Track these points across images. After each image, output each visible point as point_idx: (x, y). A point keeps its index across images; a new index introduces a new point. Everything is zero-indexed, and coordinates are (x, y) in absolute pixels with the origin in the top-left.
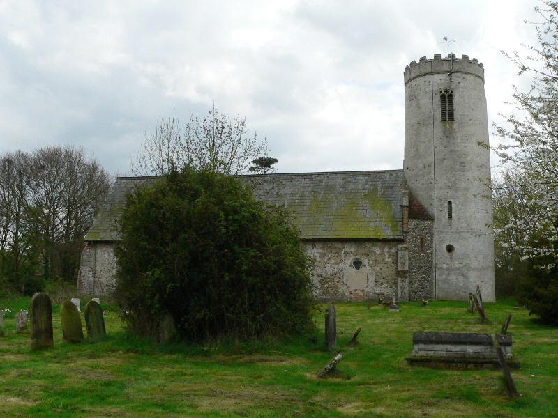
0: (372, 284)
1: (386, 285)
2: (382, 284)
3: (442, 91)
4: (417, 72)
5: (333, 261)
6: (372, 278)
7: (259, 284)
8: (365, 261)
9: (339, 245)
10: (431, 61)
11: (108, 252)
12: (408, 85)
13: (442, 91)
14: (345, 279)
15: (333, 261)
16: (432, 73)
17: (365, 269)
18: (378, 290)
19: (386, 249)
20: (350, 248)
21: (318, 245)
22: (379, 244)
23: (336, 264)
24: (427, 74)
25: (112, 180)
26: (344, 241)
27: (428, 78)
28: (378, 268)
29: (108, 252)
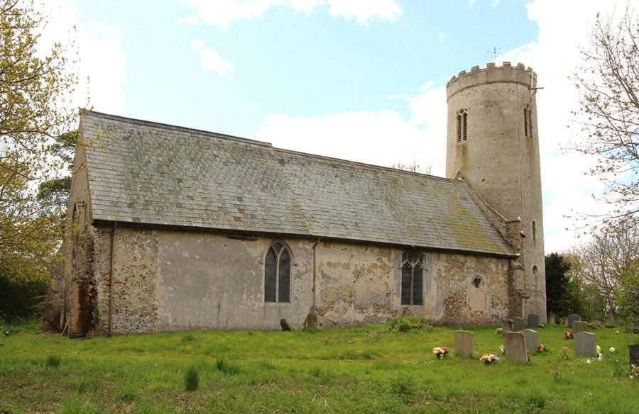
0: (489, 305)
1: (499, 306)
2: (497, 305)
3: (497, 106)
4: (466, 81)
5: (457, 277)
6: (489, 298)
7: (52, 254)
8: (484, 278)
9: (461, 259)
10: (501, 68)
11: (141, 246)
12: (450, 101)
13: (497, 106)
14: (467, 298)
15: (457, 277)
16: (517, 83)
17: (483, 288)
18: (494, 311)
19: (500, 267)
20: (471, 262)
21: (443, 257)
22: (494, 260)
23: (459, 280)
24: (511, 82)
25: (528, 6)
26: (466, 254)
27: (511, 86)
28: (494, 287)
29: (141, 246)
